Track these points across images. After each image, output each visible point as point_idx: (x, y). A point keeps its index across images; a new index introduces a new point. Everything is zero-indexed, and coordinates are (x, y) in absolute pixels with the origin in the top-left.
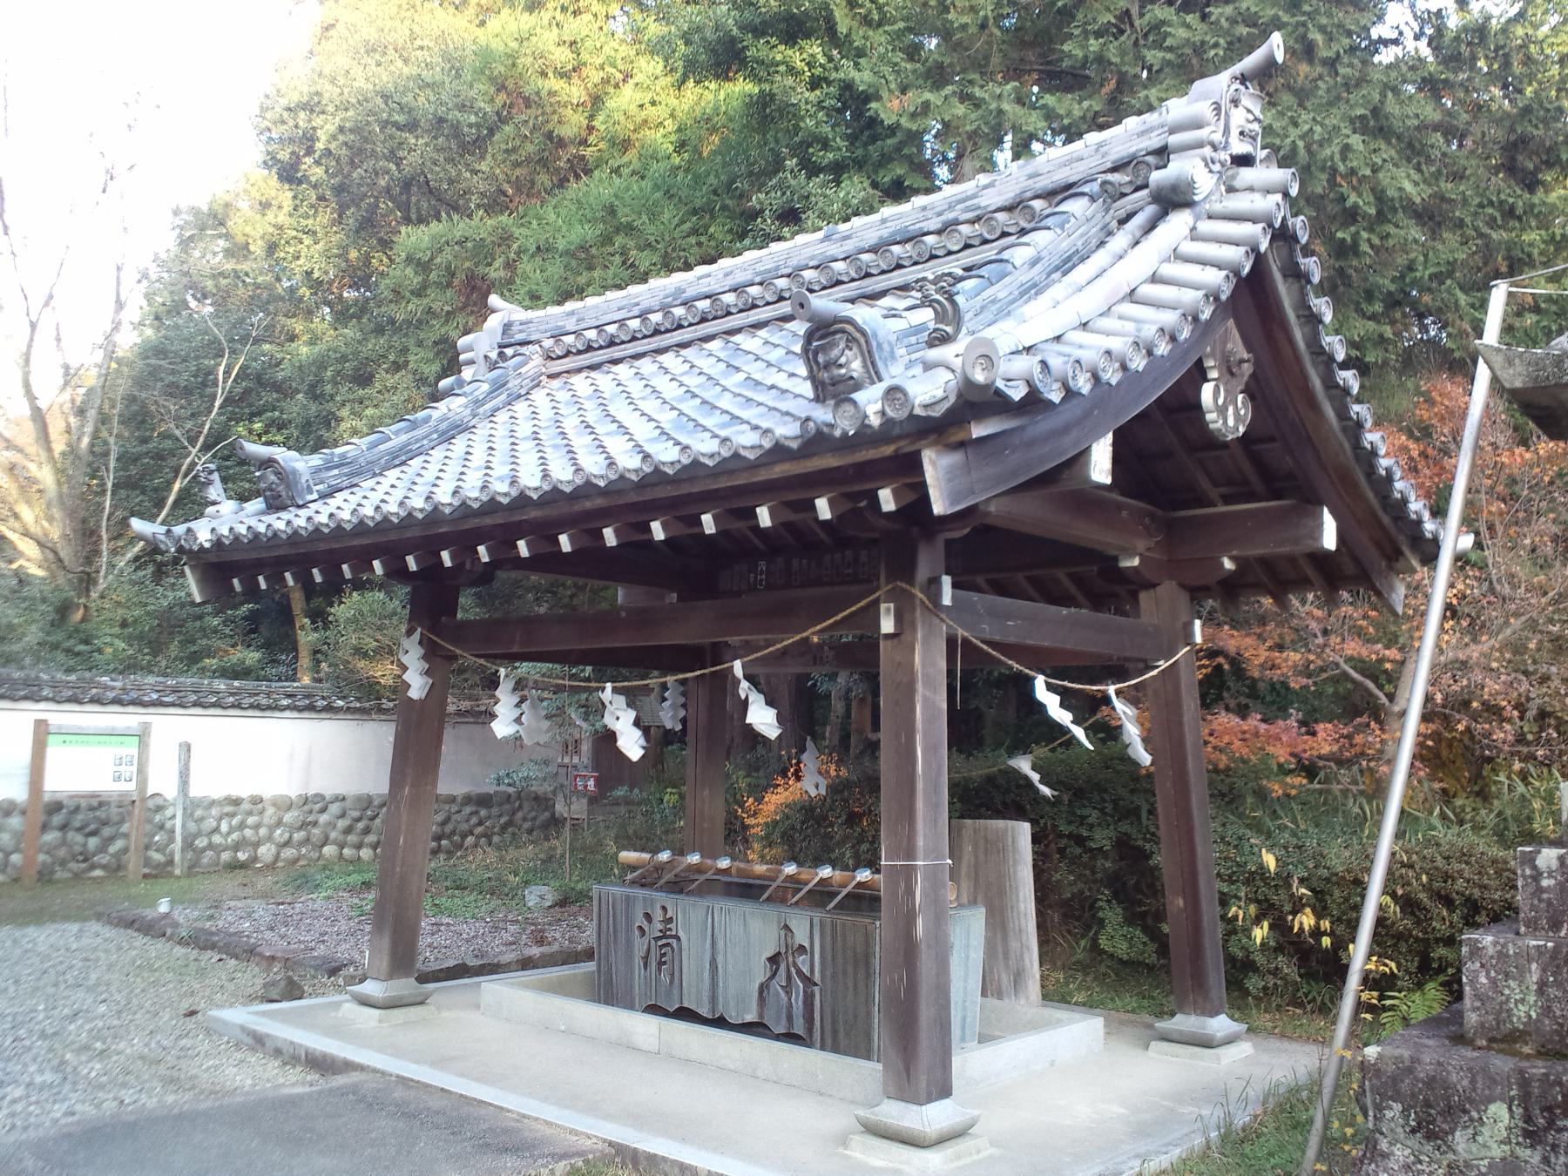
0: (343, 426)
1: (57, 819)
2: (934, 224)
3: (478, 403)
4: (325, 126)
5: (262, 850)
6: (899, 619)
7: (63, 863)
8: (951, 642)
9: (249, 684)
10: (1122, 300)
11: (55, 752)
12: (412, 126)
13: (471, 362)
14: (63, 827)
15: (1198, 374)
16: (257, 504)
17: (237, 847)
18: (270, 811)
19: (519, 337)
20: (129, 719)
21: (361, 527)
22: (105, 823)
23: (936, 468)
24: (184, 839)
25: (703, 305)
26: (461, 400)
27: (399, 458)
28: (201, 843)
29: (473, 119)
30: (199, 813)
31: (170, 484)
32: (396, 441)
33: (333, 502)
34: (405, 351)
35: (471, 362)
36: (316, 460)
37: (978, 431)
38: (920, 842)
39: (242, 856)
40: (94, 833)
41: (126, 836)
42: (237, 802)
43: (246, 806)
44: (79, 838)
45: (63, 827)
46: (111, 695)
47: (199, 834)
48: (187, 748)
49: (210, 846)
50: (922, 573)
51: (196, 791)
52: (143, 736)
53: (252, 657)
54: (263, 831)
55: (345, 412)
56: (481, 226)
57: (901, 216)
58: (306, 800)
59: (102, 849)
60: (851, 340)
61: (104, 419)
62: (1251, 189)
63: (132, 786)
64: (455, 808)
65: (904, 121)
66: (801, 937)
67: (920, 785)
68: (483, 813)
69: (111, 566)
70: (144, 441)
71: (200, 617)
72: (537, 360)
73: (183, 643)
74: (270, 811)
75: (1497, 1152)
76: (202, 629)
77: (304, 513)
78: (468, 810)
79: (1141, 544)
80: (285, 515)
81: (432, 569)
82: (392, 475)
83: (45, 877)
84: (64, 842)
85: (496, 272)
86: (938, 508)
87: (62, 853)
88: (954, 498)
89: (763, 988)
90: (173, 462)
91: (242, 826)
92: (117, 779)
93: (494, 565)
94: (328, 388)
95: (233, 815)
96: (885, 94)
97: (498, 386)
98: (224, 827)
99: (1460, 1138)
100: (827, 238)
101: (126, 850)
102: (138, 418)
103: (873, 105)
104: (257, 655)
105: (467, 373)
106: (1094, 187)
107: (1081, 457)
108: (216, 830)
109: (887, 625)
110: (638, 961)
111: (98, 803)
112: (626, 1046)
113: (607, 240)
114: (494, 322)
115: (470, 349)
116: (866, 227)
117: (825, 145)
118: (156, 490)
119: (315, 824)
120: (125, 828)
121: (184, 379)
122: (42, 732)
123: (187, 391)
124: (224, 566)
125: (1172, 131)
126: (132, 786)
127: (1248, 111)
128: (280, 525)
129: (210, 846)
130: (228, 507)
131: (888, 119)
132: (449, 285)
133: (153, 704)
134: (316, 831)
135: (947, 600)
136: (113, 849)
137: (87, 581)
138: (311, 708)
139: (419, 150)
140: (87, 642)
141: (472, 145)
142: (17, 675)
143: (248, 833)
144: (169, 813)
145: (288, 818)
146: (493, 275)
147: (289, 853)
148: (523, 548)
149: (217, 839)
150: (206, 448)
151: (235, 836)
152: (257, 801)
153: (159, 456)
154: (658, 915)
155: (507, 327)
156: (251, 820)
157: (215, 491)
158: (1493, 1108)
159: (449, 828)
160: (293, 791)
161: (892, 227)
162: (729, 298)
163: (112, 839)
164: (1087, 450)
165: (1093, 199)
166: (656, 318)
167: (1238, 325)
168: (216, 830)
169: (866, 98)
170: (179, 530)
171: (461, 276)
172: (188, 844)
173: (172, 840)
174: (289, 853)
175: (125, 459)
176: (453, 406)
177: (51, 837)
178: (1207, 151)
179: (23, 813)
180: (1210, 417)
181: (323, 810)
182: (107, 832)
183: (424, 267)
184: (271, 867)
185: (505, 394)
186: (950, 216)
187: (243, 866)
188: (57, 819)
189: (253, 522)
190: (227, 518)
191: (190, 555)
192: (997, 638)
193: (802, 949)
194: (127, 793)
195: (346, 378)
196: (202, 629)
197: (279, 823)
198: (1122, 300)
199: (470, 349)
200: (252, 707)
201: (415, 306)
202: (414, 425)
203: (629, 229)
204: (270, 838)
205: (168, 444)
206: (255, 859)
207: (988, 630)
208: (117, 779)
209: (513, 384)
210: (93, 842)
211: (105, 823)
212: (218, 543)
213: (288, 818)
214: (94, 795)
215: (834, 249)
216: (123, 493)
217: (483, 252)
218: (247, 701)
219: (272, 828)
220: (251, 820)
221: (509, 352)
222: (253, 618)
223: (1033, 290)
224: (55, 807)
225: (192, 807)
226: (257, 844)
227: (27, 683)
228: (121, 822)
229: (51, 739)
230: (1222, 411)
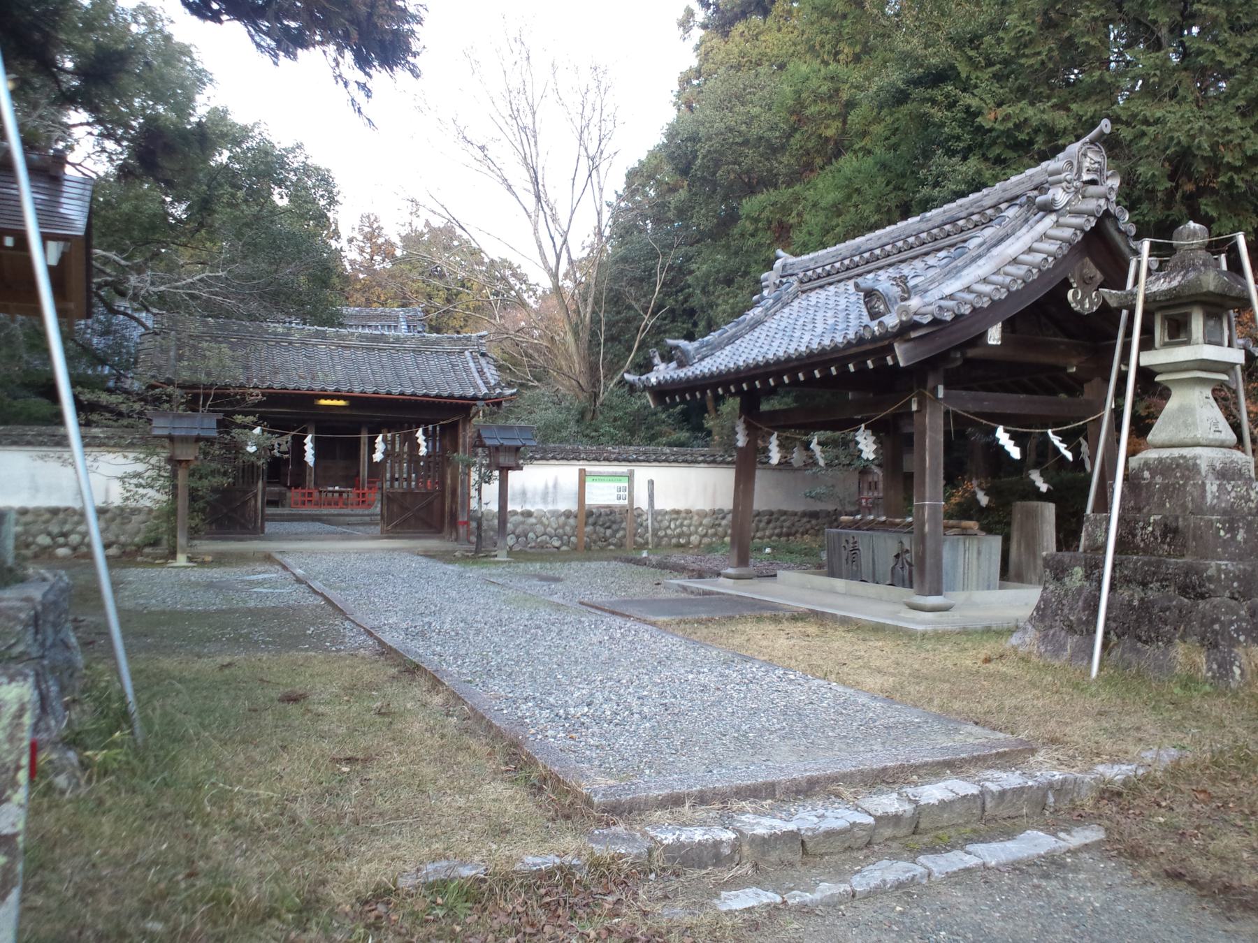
0: (720, 308)
1: (591, 520)
2: (963, 214)
3: (768, 309)
4: (703, 149)
5: (692, 538)
6: (920, 404)
7: (595, 542)
8: (947, 413)
9: (682, 449)
10: (1009, 263)
11: (589, 484)
12: (746, 143)
13: (767, 287)
14: (594, 524)
15: (1066, 285)
16: (673, 365)
17: (679, 536)
18: (696, 518)
19: (790, 272)
20: (623, 468)
21: (712, 375)
22: (614, 522)
23: (899, 349)
24: (653, 530)
25: (866, 255)
26: (760, 309)
27: (732, 340)
28: (661, 533)
29: (778, 134)
30: (659, 518)
31: (633, 338)
32: (730, 332)
33: (703, 363)
34: (749, 266)
35: (767, 287)
36: (696, 344)
37: (913, 335)
38: (927, 495)
39: (682, 541)
40: (609, 527)
41: (624, 529)
42: (678, 512)
43: (683, 515)
44: (602, 530)
45: (594, 524)
46: (613, 456)
47: (660, 529)
48: (651, 483)
49: (666, 535)
50: (930, 384)
51: (658, 506)
52: (630, 477)
53: (684, 435)
54: (692, 528)
55: (720, 301)
56: (783, 194)
57: (951, 209)
58: (714, 512)
59: (613, 535)
60: (879, 299)
61: (597, 302)
62: (1092, 197)
63: (626, 502)
64: (796, 518)
65: (996, 126)
66: (907, 546)
67: (927, 472)
68: (814, 522)
69: (606, 387)
70: (619, 313)
71: (655, 414)
72: (796, 284)
73: (647, 428)
74: (696, 518)
75: (1078, 584)
76: (657, 421)
77: (692, 369)
78: (805, 520)
79: (1075, 361)
80: (685, 370)
81: (752, 388)
82: (728, 348)
83: (588, 548)
84: (595, 532)
85: (792, 220)
86: (902, 364)
87: (594, 537)
88: (906, 360)
89: (893, 568)
90: (636, 324)
91: (682, 525)
92: (619, 498)
93: (776, 386)
94: (711, 288)
95: (676, 519)
96: (986, 112)
97: (777, 300)
98: (672, 526)
99: (1067, 580)
100: (921, 220)
101: (624, 536)
102: (616, 299)
103: (979, 119)
104: (687, 434)
105: (765, 293)
106: (1024, 199)
107: (984, 334)
108: (669, 527)
109: (914, 407)
110: (844, 561)
111: (611, 511)
112: (833, 591)
113: (849, 197)
114: (778, 264)
115: (766, 280)
116: (938, 215)
117: (958, 138)
118: (627, 341)
119: (719, 525)
120: (624, 525)
121: (638, 273)
122: (583, 475)
123: (642, 280)
124: (662, 392)
125: (1050, 175)
126: (626, 502)
127: (1094, 158)
128: (682, 375)
129: (666, 535)
130: (662, 366)
131: (987, 126)
132: (769, 228)
133: (634, 461)
134: (720, 529)
135: (941, 394)
136: (618, 535)
137: (596, 396)
138: (714, 462)
139: (750, 157)
140: (596, 431)
141: (775, 150)
142: (568, 447)
143: (685, 529)
144: (644, 517)
145: (705, 521)
146: (791, 221)
147: (706, 540)
148: (786, 379)
149: (669, 532)
150: (654, 313)
151: (678, 530)
152: (688, 512)
153: (628, 321)
154: (851, 541)
155: (784, 266)
156: (686, 522)
157: (657, 360)
158: (1076, 569)
159: (793, 530)
160: (707, 507)
161: (948, 215)
162: (878, 252)
163: (617, 531)
164: (985, 333)
165: (1021, 206)
166: (847, 262)
167: (1093, 260)
168: (669, 527)
169: (979, 113)
170: (644, 378)
171: (775, 224)
172: (655, 534)
173: (647, 531)
174: (706, 540)
175: (610, 325)
176: (756, 312)
177: (589, 529)
178: (1064, 184)
179: (576, 517)
180: (1073, 305)
181: (723, 518)
182: (614, 527)
183: (756, 220)
184: (698, 546)
185: (781, 302)
186: (971, 210)
187: (682, 546)
188: (591, 520)
189: (672, 373)
190: (662, 372)
191: (646, 388)
192: (977, 410)
193: (907, 551)
194: (623, 506)
195: (720, 282)
196: (657, 421)
197: (701, 524)
198: (1009, 263)
199: (766, 280)
200: (683, 461)
201: (751, 242)
202: (738, 324)
203: (858, 191)
204: (696, 532)
205: (632, 313)
206: (689, 543)
207: (971, 407)
208: (619, 498)
209: (785, 298)
210: (609, 532)
211: (614, 522)
212: (659, 383)
213: (705, 521)
214: (608, 507)
215: (924, 226)
216: (609, 344)
217: (785, 209)
218: (681, 459)
219: (697, 527)
220: (686, 522)
221: (784, 280)
222: (683, 412)
223: (974, 260)
224: (590, 514)
225: (656, 514)
226: (690, 535)
227: (573, 451)
228: (622, 522)
229: (588, 479)
230: (1081, 302)
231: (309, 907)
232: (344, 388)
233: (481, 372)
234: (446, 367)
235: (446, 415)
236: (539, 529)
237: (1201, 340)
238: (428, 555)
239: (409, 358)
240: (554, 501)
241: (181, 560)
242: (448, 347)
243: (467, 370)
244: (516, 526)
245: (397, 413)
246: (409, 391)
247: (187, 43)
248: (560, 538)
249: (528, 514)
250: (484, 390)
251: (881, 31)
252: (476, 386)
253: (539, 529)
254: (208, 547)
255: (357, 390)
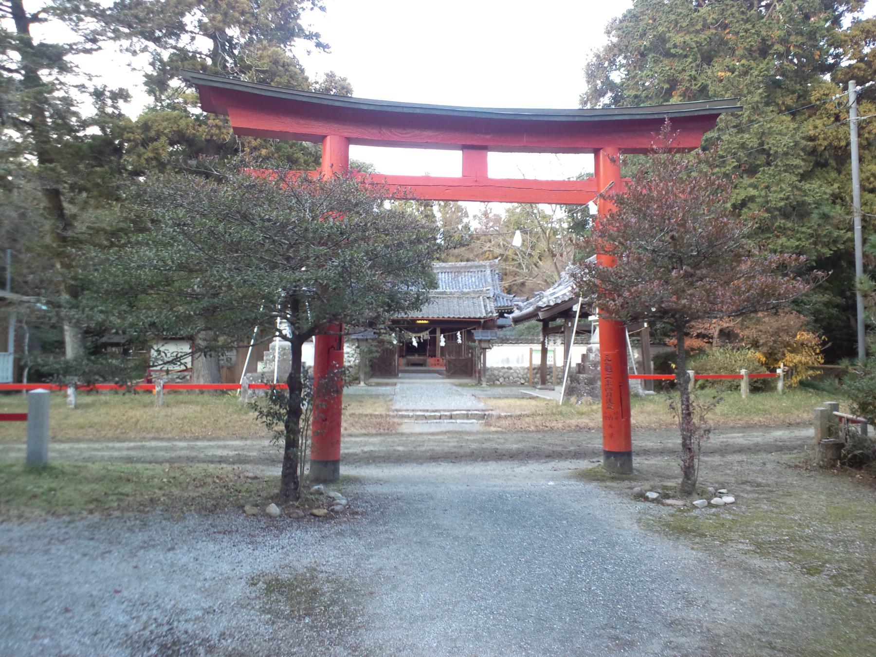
23: (540, 314)
231: (870, 562)
232: (425, 316)
233: (485, 306)
234: (471, 304)
235: (468, 325)
236: (515, 375)
237: (78, 402)
238: (460, 385)
239: (455, 301)
240: (522, 362)
241: (362, 384)
242: (473, 295)
243: (480, 305)
244: (504, 373)
245: (449, 326)
246: (452, 316)
247: (368, 162)
248: (524, 379)
249: (510, 368)
250: (484, 315)
251: (212, 291)
252: (481, 313)
253: (515, 375)
254: (374, 380)
255: (430, 317)
